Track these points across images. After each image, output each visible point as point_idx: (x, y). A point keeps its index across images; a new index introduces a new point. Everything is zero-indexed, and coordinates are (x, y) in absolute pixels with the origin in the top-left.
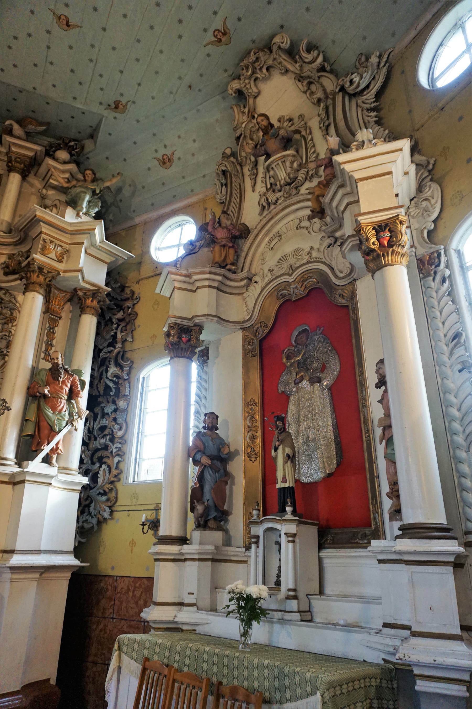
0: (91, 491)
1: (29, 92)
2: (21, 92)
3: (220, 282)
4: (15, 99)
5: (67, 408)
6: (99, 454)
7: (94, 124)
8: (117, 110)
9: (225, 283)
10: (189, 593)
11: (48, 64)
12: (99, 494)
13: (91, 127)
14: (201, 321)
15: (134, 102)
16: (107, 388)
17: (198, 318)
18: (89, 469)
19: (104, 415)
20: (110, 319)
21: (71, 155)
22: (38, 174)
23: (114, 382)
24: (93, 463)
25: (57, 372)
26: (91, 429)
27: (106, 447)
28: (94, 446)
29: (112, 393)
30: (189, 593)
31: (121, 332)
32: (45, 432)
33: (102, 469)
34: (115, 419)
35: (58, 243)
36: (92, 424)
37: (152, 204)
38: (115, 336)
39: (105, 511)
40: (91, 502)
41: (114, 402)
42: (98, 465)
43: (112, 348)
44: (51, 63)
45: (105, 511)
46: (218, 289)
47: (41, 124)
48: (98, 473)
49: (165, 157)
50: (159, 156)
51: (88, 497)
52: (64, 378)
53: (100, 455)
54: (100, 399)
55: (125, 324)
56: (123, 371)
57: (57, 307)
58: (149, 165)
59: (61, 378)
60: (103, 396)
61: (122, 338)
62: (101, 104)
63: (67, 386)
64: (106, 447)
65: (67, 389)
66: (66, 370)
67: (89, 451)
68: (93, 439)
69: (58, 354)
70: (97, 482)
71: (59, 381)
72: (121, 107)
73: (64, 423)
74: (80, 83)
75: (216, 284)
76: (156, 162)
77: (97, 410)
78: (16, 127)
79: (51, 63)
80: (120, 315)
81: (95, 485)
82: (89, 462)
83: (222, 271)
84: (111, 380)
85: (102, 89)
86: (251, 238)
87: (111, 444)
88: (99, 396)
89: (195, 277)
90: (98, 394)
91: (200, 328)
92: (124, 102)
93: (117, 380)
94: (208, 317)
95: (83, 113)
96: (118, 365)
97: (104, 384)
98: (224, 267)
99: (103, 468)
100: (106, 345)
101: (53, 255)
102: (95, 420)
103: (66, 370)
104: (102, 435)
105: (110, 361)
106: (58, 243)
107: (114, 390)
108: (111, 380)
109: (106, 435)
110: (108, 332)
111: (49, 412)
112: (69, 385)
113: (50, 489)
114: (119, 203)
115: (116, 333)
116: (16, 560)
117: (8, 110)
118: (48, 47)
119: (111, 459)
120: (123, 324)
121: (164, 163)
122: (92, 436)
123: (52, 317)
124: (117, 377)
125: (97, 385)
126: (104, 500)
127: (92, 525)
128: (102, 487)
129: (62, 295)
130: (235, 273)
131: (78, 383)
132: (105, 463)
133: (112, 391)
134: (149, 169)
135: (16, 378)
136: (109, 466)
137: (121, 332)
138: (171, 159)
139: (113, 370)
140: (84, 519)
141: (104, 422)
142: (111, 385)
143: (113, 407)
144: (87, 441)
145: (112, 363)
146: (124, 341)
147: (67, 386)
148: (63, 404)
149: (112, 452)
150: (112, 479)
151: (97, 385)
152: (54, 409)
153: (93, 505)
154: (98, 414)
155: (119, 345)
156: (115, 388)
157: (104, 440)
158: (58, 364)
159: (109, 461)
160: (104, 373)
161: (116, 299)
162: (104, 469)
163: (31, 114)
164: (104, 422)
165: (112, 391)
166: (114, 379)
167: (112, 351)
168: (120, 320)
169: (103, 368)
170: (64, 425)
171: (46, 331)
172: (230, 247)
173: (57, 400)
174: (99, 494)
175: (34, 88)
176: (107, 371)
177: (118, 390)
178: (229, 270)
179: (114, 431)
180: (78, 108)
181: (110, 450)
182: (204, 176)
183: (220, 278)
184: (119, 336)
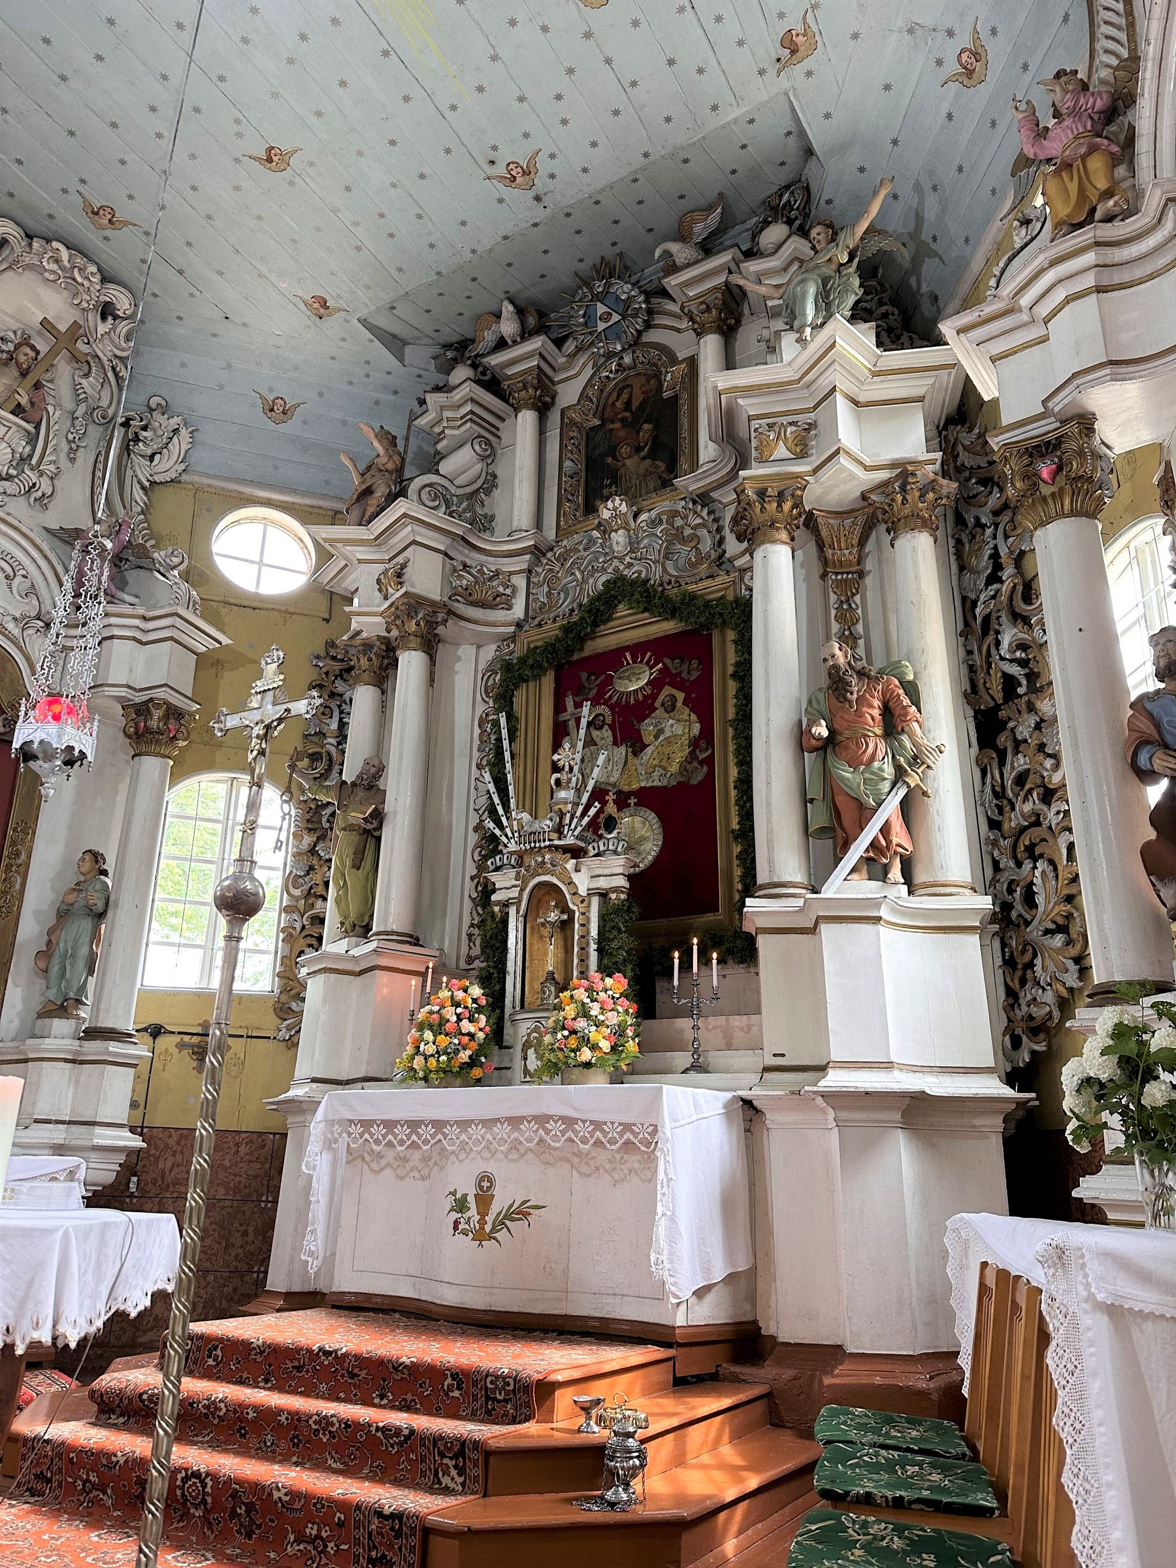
0: (1028, 930)
1: (644, 169)
2: (635, 180)
3: (1097, 266)
4: (640, 202)
5: (886, 753)
6: (1025, 840)
7: (788, 124)
8: (798, 54)
9: (1116, 260)
10: (775, 1055)
11: (629, 90)
12: (1047, 932)
13: (789, 133)
14: (1065, 401)
15: (814, 7)
16: (1009, 683)
17: (1057, 399)
18: (1013, 880)
19: (1018, 744)
20: (978, 524)
21: (790, 222)
22: (753, 309)
23: (1023, 663)
24: (1019, 864)
25: (840, 685)
26: (997, 789)
27: (1036, 821)
28: (1013, 824)
29: (1021, 691)
30: (775, 1055)
31: (1006, 537)
32: (848, 818)
33: (1037, 873)
34: (1041, 747)
35: (785, 420)
36: (997, 776)
37: (994, 192)
38: (995, 556)
39: (1067, 971)
40: (1035, 955)
41: (1031, 708)
42: (1028, 865)
43: (996, 586)
44: (634, 84)
45: (1067, 971)
46: (1100, 289)
47: (710, 209)
48: (1032, 883)
49: (964, 56)
50: (952, 67)
51: (1026, 944)
52: (858, 692)
53: (1027, 843)
54: (1002, 714)
55: (1011, 514)
56: (1030, 626)
57: (847, 552)
58: (945, 109)
59: (852, 694)
60: (1006, 702)
61: (1012, 552)
62: (762, 72)
63: (872, 707)
64: (1036, 821)
65: (876, 713)
66: (861, 674)
67: (1005, 839)
68: (1008, 808)
69: (832, 646)
70: (1036, 907)
71: (850, 702)
72: (800, 40)
73: (886, 787)
74: (700, 71)
75: (1089, 281)
76: (954, 87)
77: (1003, 740)
78: (674, 247)
79: (634, 84)
80: (994, 500)
81: (1034, 911)
82: (1012, 864)
83: (1085, 236)
84: (1011, 661)
85: (741, 43)
86: (1147, 83)
87: (1045, 808)
88: (997, 708)
89: (1025, 301)
90: (992, 704)
91: (1086, 422)
92: (800, 28)
93: (1023, 655)
94: (1079, 381)
95: (751, 121)
96: (1019, 618)
97: (999, 675)
98: (1090, 219)
99: (1040, 869)
100: (981, 583)
101: (781, 451)
102: (1002, 763)
103: (861, 674)
104: (1022, 794)
105: (998, 618)
106: (785, 420)
107: (1024, 682)
108: (1011, 661)
109: (1030, 791)
110: (978, 553)
111: (847, 773)
112: (877, 703)
113: (882, 929)
114: (932, 245)
115: (996, 548)
116: (834, 1080)
117: (650, 230)
118: (608, 61)
119: (1050, 843)
120: (1005, 518)
121: (970, 73)
122: (1005, 802)
123: (839, 577)
124: (1023, 647)
125: (985, 683)
126: (1059, 944)
127: (1048, 1008)
128: (1047, 914)
129: (848, 522)
130: (1127, 214)
131: (901, 691)
132: (1041, 856)
133: (1020, 685)
134: (950, 117)
135: (767, 725)
136: (1052, 862)
137: (1006, 537)
138: (980, 51)
139: (1009, 635)
140: (1029, 997)
141: (1022, 762)
142: (1014, 670)
143: (1032, 720)
144: (997, 818)
145: (1004, 619)
146: (1020, 558)
147: (872, 707)
148: (876, 745)
149: (1050, 828)
150: (1066, 891)
151: (985, 683)
152: (854, 764)
153: (1038, 961)
154: (1006, 748)
155: (1008, 572)
156: (1025, 675)
157: (1031, 803)
158: (836, 667)
159: (1048, 852)
160: (993, 651)
161: (979, 467)
162: (1043, 872)
163: (686, 205)
164: (1022, 762)
165: (1020, 685)
166: (1018, 654)
167: (997, 591)
168: (996, 513)
169: (990, 639)
170: (887, 790)
171: (833, 612)
172: (1084, 158)
173: (857, 742)
174: (1047, 932)
175: (646, 155)
176: (998, 644)
177: (1032, 677)
178: (1109, 219)
179: (1045, 774)
180: (735, 121)
181: (1045, 824)
182: (1066, 19)
183: (1090, 258)
184: (1003, 551)
